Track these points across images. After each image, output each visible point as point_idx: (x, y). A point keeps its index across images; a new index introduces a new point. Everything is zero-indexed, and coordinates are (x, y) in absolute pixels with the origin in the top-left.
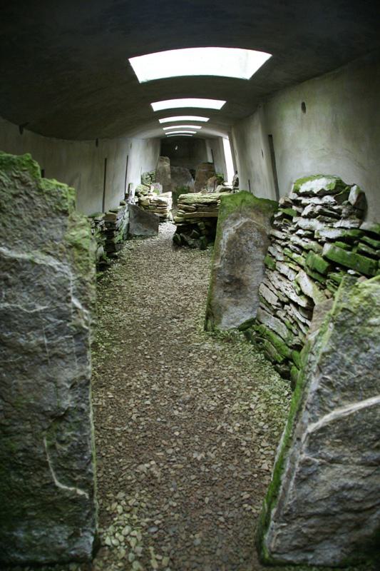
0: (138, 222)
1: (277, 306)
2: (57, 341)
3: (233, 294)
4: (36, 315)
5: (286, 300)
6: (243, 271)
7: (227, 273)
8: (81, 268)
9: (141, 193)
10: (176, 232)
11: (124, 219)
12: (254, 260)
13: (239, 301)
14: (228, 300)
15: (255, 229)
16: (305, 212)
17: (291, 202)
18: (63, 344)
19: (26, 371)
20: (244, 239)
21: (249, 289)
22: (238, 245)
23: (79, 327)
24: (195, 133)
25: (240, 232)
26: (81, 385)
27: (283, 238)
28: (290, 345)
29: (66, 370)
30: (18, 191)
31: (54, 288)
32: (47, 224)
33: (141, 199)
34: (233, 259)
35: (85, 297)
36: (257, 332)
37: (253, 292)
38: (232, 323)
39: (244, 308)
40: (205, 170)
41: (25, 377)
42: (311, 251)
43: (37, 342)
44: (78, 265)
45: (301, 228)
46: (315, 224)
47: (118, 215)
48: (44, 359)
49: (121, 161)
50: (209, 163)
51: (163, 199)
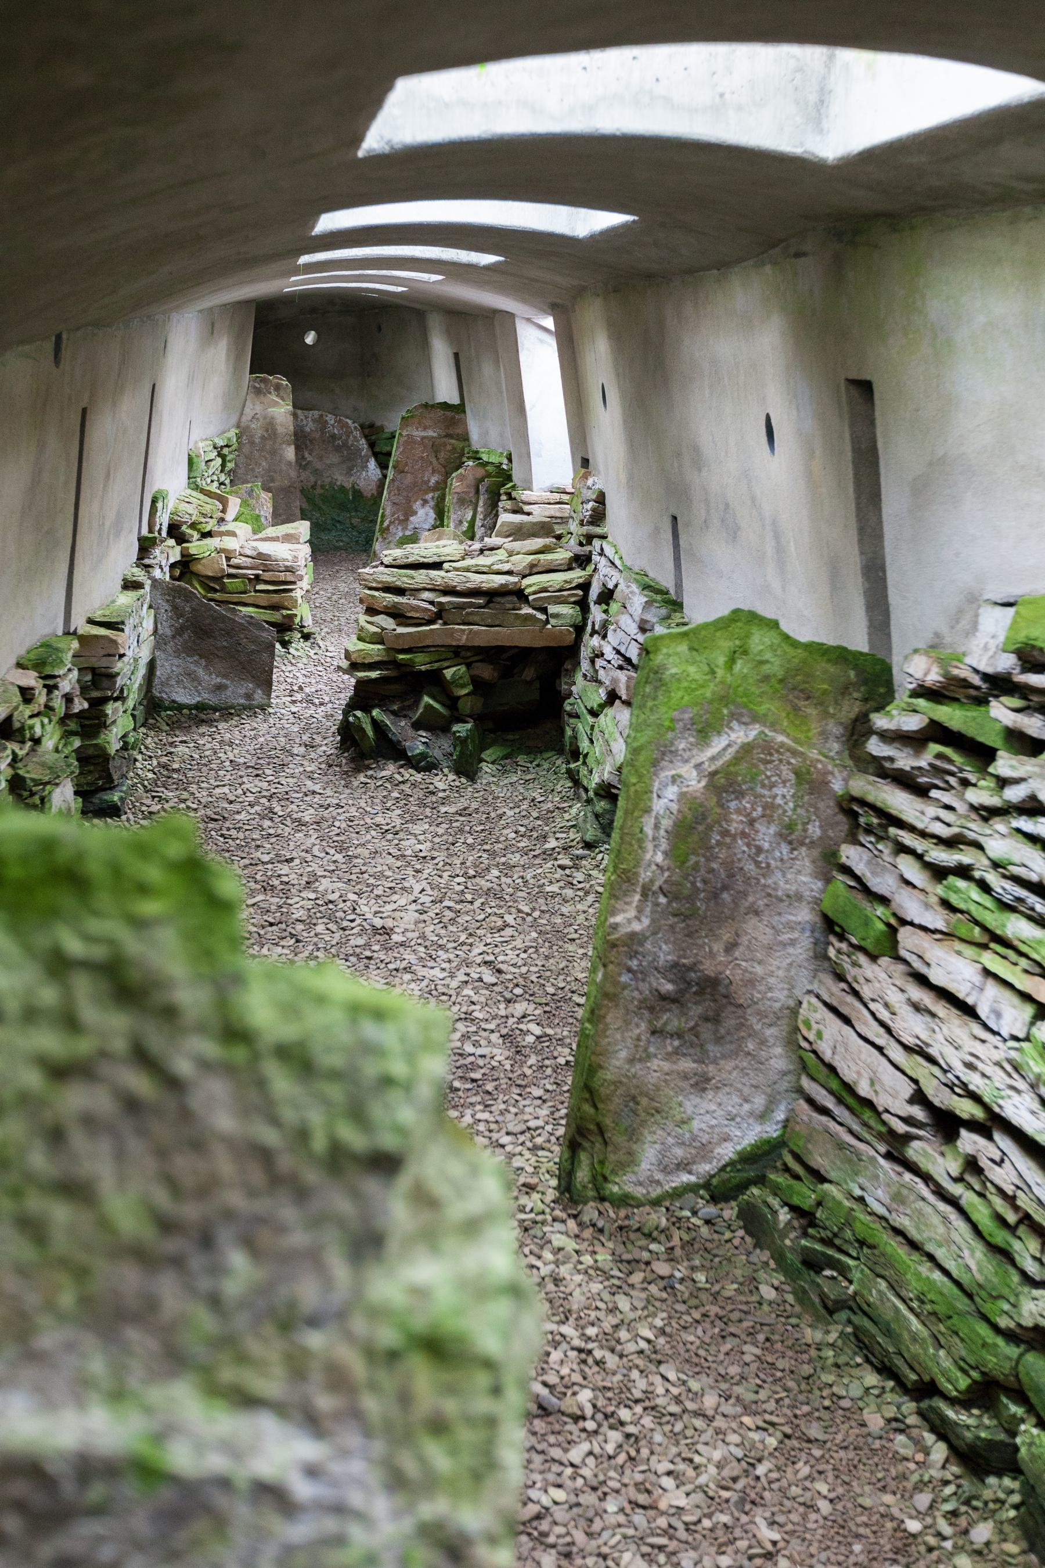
0: (188, 650)
1: (908, 1120)
3: (689, 1041)
5: (966, 1108)
7: (665, 953)
9: (193, 526)
10: (352, 706)
12: (775, 900)
13: (711, 1069)
14: (666, 1066)
15: (787, 773)
17: (976, 680)
20: (738, 811)
21: (753, 1020)
22: (716, 837)
25: (724, 783)
27: (944, 831)
28: (1003, 1322)
30: (84, 1046)
34: (691, 898)
36: (805, 1216)
37: (769, 1032)
38: (683, 1166)
39: (732, 1102)
40: (430, 433)
49: (129, 407)
50: (445, 406)
51: (281, 552)
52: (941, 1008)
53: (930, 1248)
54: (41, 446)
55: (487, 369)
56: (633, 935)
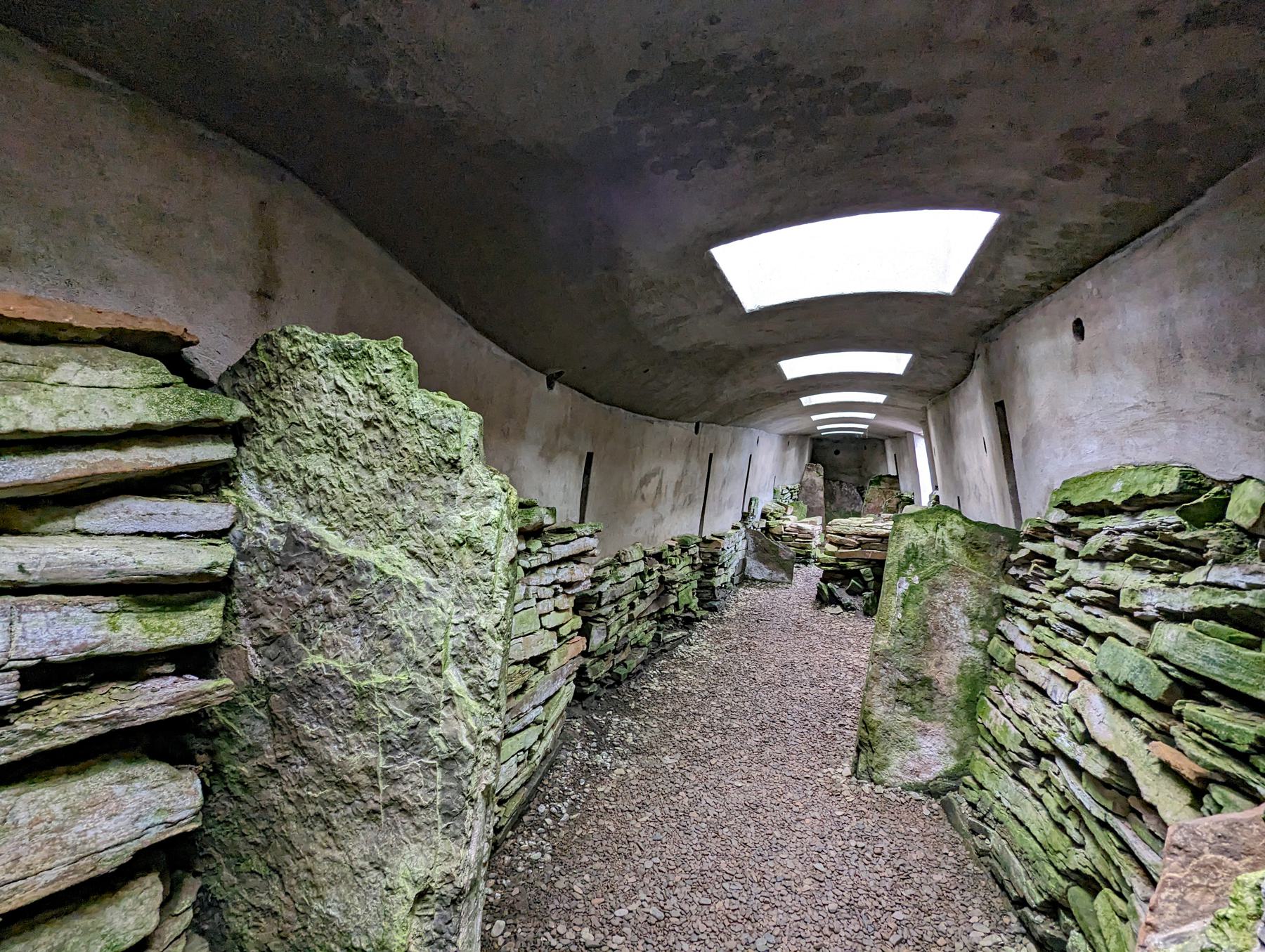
1: (1019, 755)
2: (404, 767)
3: (916, 709)
4: (364, 695)
5: (1044, 746)
6: (938, 664)
8: (476, 596)
11: (735, 549)
16: (1095, 543)
18: (414, 778)
19: (334, 829)
23: (451, 740)
24: (866, 427)
26: (441, 898)
28: (1060, 866)
29: (413, 846)
31: (410, 634)
32: (418, 489)
33: (770, 523)
35: (476, 669)
41: (331, 841)
42: (1110, 638)
43: (364, 760)
44: (471, 587)
45: (1078, 584)
46: (1122, 576)
47: (725, 543)
48: (372, 805)
52: (1034, 694)
53: (1027, 824)
54: (688, 461)
55: (906, 460)
56: (887, 651)
